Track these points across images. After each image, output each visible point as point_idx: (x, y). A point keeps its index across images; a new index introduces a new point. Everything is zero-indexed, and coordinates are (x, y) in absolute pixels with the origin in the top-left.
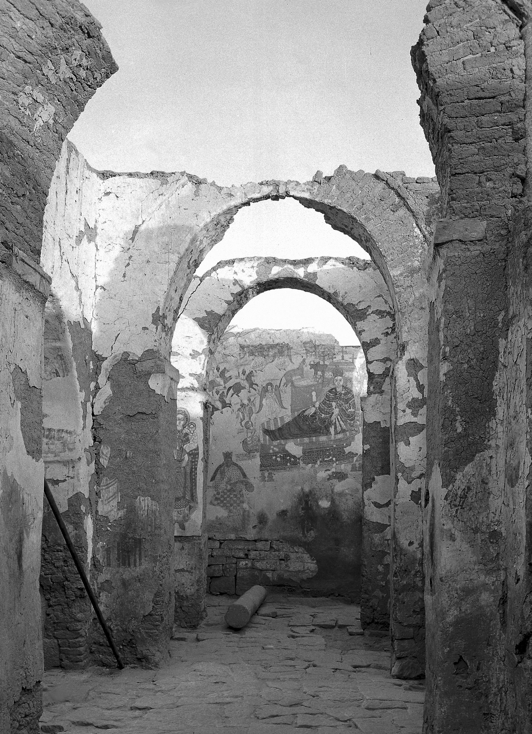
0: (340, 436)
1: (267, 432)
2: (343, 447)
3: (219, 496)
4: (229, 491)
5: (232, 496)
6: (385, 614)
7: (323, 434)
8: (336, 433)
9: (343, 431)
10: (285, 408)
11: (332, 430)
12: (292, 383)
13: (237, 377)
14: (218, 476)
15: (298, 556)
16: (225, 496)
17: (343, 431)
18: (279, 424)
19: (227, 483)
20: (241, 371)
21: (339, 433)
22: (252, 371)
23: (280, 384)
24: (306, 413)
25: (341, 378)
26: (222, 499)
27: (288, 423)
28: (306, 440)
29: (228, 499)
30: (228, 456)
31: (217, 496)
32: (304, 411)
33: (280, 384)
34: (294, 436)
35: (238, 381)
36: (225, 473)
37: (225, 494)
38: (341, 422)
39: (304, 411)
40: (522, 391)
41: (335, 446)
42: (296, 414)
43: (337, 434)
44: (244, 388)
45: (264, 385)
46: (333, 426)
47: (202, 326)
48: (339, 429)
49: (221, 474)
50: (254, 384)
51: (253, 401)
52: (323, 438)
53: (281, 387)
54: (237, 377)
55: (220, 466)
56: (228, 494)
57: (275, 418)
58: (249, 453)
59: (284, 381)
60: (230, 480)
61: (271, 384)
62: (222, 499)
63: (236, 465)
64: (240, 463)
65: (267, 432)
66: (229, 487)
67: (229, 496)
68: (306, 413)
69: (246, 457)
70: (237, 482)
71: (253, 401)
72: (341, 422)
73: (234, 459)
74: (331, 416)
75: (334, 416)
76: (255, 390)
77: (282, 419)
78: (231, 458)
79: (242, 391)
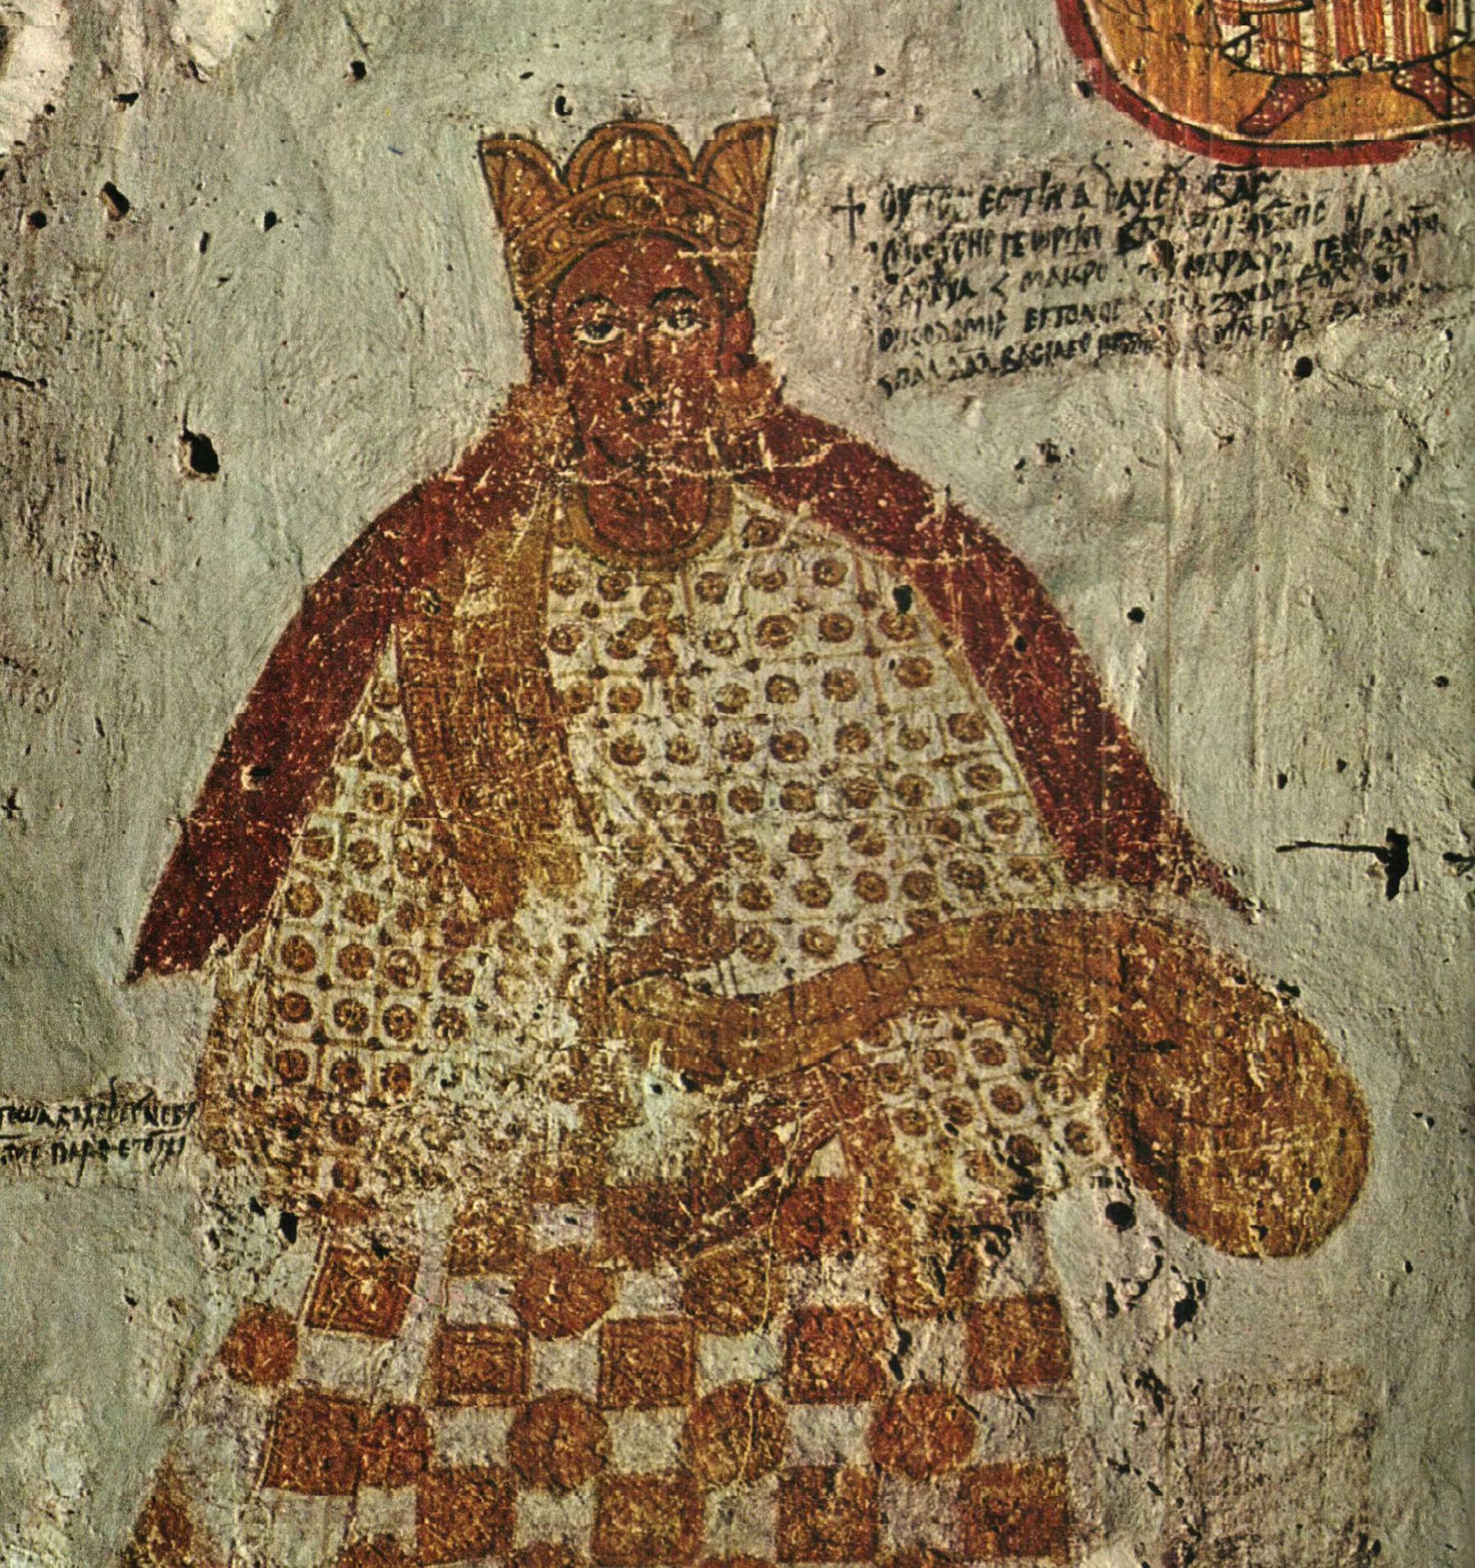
3: (399, 1369)
4: (649, 1221)
5: (735, 1359)
6: (791, 997)
14: (362, 811)
16: (566, 1365)
18: (1432, 44)
19: (603, 996)
26: (474, 1435)
29: (644, 1442)
30: (626, 233)
31: (338, 1361)
36: (547, 718)
37: (560, 1296)
40: (1269, 698)
49: (440, 747)
55: (427, 529)
56: (645, 1292)
58: (1249, 161)
60: (706, 937)
62: (474, 1435)
63: (873, 497)
64: (956, 448)
66: (665, 1121)
67: (647, 1369)
69: (1129, 283)
70: (875, 992)
73: (812, 307)
78: (727, 299)
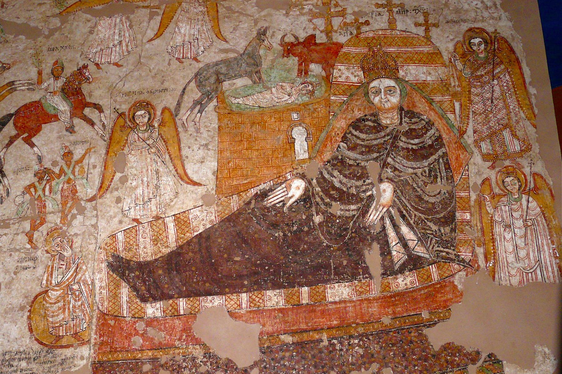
0: (404, 282)
1: (121, 267)
2: (420, 325)
7: (340, 275)
8: (390, 270)
9: (414, 263)
10: (195, 184)
11: (373, 257)
12: (222, 100)
13: (32, 86)
15: (94, 137)
17: (414, 263)
20: (47, 69)
21: (401, 271)
22: (85, 67)
23: (179, 104)
24: (273, 199)
25: (392, 83)
27: (205, 238)
28: (274, 298)
32: (264, 195)
33: (179, 104)
34: (223, 285)
35: (35, 97)
38: (405, 229)
39: (264, 195)
41: (386, 320)
42: (235, 203)
43: (395, 273)
44: (55, 117)
45: (124, 108)
46: (376, 246)
47: (34, 144)
48: (398, 254)
50: (88, 105)
51: (81, 161)
52: (339, 292)
53: (184, 115)
54: (32, 86)
57: (157, 218)
59: (194, 94)
61: (147, 106)
65: (121, 267)
68: (273, 199)
71: (81, 161)
72: (405, 229)
74: (364, 212)
75: (373, 217)
76: (92, 124)
77: (181, 221)
79: (46, 128)
